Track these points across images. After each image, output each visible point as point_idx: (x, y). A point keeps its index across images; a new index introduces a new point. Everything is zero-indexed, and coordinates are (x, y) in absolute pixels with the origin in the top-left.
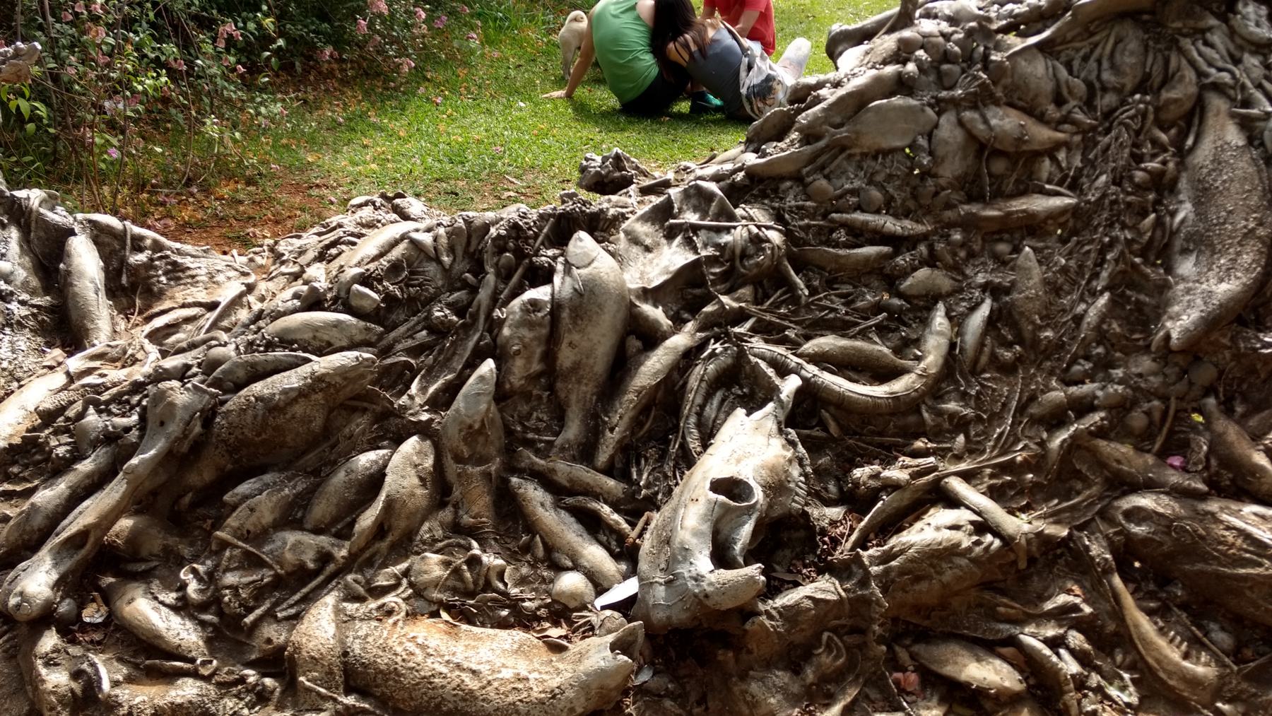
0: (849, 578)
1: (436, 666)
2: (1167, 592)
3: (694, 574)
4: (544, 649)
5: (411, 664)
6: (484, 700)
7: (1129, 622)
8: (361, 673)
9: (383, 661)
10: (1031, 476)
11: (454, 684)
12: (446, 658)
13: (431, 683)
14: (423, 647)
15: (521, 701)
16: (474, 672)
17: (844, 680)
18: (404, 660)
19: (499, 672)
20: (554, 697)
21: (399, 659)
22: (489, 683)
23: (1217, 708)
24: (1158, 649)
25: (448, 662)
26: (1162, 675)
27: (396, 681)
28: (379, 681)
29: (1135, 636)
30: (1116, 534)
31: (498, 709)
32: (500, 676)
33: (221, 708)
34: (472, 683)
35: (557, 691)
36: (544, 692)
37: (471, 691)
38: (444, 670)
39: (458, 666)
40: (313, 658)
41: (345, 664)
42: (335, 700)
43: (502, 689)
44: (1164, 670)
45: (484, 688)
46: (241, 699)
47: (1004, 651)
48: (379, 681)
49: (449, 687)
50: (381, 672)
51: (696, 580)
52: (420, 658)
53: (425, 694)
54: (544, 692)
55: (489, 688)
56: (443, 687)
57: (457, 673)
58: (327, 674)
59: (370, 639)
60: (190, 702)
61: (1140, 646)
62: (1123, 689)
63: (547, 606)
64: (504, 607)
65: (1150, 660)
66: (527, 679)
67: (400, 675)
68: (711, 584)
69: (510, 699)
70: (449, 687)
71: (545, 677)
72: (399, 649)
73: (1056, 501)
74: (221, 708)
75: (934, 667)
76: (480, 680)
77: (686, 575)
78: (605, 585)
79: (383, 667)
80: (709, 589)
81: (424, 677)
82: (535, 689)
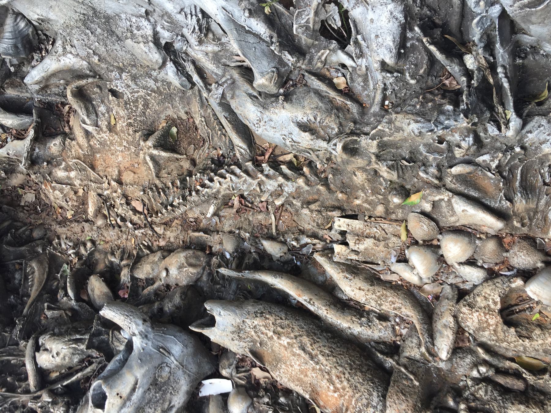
0: (103, 341)
1: (325, 362)
2: (16, 301)
3: (145, 341)
4: (266, 358)
5: (340, 369)
6: (303, 328)
7: (37, 293)
8: (376, 378)
9: (358, 379)
10: (8, 379)
11: (316, 345)
12: (318, 367)
13: (332, 352)
14: (330, 381)
15: (281, 319)
16: (304, 350)
17: (146, 299)
18: (344, 374)
19: (288, 343)
20: (262, 313)
21: (347, 375)
22: (296, 337)
23: (43, 251)
24: (39, 278)
25: (317, 363)
26: (47, 269)
27: (354, 362)
28: (366, 368)
29: (41, 287)
30: (6, 332)
31: (296, 320)
32: (289, 341)
33: (489, 393)
34: (306, 340)
35: (259, 315)
36: (267, 319)
37: (308, 336)
38: (320, 357)
39: (312, 357)
40: (404, 395)
41: (386, 390)
42: (398, 364)
43: (289, 330)
44: (44, 270)
45: (300, 336)
46: (472, 394)
47: (85, 298)
48: (366, 368)
49: (321, 344)
50: (361, 372)
51: (146, 336)
52: (334, 371)
53: (337, 347)
54: (267, 319)
55: (297, 334)
56: (324, 346)
57: (314, 353)
58: (397, 381)
59: (365, 401)
60: (513, 404)
61: (44, 282)
62: (64, 271)
63: (258, 397)
64: (280, 404)
65: (45, 276)
66: (274, 332)
67: (350, 365)
68: (137, 325)
69: (287, 322)
70: (321, 344)
71: (263, 329)
72: (345, 383)
73: (12, 362)
74: (489, 393)
75: (111, 294)
76: (301, 342)
77: (150, 343)
78: (220, 398)
79: (359, 374)
80: (140, 322)
81: (334, 357)
82: (271, 322)
